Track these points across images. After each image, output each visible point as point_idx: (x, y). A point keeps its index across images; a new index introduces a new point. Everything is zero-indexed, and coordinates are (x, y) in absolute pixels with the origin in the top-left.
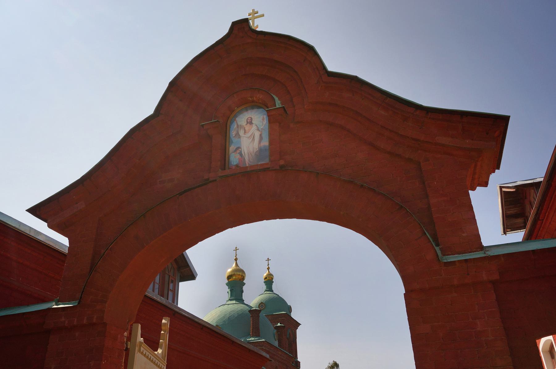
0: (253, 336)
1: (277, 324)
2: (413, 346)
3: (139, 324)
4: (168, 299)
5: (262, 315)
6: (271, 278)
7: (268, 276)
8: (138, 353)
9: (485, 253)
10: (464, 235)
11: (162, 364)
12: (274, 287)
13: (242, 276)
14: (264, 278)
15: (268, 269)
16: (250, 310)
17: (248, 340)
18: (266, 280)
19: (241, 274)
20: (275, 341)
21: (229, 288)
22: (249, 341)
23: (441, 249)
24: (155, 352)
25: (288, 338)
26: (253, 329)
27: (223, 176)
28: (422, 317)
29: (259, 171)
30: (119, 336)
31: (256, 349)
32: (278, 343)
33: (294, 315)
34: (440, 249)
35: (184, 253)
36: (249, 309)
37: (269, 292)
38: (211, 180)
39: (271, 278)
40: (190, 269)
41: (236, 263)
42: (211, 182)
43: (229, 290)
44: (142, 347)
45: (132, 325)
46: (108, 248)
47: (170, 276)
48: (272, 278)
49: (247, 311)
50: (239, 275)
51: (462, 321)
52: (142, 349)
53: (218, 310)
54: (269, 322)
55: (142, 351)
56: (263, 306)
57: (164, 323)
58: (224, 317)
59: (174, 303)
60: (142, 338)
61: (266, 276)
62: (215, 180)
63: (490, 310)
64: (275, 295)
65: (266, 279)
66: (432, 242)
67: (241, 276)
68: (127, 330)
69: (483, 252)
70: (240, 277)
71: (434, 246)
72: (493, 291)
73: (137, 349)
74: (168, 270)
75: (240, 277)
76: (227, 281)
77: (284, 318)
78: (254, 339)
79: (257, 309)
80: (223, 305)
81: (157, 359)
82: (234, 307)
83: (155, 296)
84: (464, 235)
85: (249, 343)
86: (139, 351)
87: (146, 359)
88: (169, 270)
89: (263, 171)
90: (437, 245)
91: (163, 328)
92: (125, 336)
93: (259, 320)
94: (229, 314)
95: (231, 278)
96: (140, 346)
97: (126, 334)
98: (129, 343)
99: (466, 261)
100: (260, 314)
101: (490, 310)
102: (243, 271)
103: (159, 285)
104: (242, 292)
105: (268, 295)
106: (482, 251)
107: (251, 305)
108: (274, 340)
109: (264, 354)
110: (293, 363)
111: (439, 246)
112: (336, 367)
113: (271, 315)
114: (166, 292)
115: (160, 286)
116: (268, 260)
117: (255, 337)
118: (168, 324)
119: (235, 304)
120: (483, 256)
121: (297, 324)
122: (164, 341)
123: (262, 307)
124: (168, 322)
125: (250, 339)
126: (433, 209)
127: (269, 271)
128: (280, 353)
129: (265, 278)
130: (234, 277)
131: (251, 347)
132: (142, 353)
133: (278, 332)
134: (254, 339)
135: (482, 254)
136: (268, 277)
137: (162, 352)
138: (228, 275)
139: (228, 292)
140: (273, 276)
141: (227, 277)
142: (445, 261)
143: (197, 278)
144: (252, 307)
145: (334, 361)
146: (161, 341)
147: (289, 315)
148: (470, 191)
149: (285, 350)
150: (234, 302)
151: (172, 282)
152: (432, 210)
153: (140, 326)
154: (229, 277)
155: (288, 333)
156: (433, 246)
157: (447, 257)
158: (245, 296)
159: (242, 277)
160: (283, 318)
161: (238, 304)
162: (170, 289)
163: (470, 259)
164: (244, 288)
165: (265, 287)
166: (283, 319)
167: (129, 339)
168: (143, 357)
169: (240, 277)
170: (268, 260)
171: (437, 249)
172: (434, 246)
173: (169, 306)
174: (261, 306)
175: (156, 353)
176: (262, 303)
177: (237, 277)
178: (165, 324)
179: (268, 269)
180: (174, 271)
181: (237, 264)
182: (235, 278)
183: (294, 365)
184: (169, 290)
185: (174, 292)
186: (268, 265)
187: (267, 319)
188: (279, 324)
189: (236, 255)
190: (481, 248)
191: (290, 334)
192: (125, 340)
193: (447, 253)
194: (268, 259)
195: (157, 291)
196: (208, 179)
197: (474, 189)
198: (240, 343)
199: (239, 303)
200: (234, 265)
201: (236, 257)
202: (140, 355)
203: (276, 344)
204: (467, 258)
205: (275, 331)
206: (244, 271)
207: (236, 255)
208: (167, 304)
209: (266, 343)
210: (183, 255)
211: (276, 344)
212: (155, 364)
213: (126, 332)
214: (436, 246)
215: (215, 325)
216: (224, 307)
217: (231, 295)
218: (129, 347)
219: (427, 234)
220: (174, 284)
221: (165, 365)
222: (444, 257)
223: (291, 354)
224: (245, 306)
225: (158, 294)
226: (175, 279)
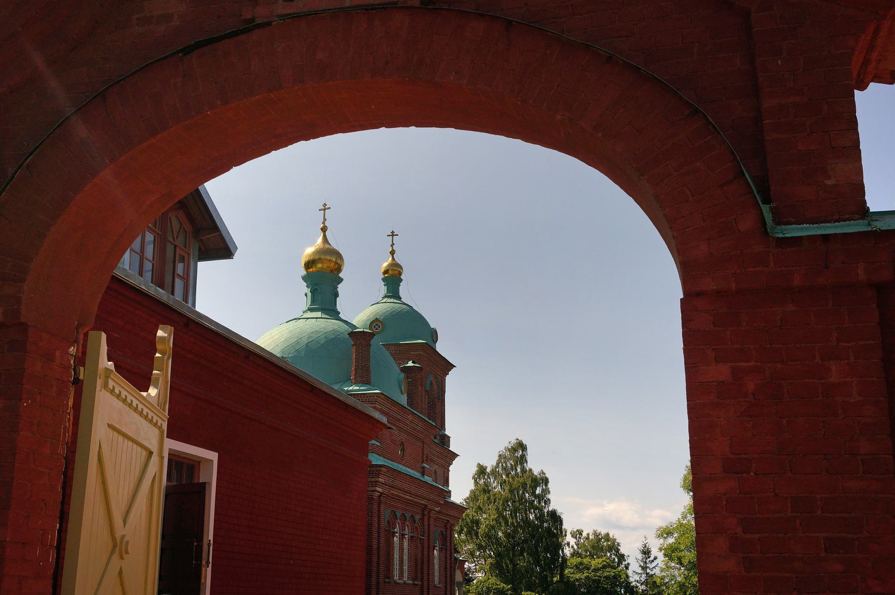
0: (356, 383)
1: (407, 363)
2: (688, 405)
3: (103, 333)
4: (173, 294)
5: (377, 343)
6: (396, 272)
7: (392, 268)
8: (102, 390)
9: (869, 225)
10: (829, 182)
11: (159, 416)
12: (403, 290)
13: (336, 263)
14: (383, 270)
15: (392, 253)
16: (352, 332)
17: (346, 389)
18: (386, 275)
19: (334, 259)
20: (402, 395)
21: (308, 287)
22: (348, 391)
23: (775, 212)
24: (142, 393)
25: (427, 391)
26: (356, 369)
27: (287, 15)
28: (714, 349)
29: (373, 9)
30: (58, 353)
31: (359, 405)
32: (408, 399)
33: (442, 348)
34: (772, 210)
35: (200, 188)
36: (350, 330)
37: (392, 300)
38: (259, 21)
39: (396, 272)
40: (221, 236)
41: (325, 236)
42: (259, 26)
43: (308, 291)
44: (112, 379)
45: (86, 335)
46: (22, 164)
47: (177, 248)
48: (400, 272)
49: (346, 333)
50: (330, 260)
51: (799, 362)
52: (111, 384)
53: (285, 328)
54: (390, 359)
55: (146, 414)
56: (379, 327)
57: (159, 337)
58: (297, 343)
59: (186, 302)
60: (111, 363)
61: (386, 267)
62: (269, 24)
63: (861, 343)
64: (404, 306)
65: (387, 273)
66: (755, 193)
67: (334, 263)
68: (75, 342)
69: (865, 222)
70: (332, 265)
71: (760, 201)
72: (875, 305)
73: (99, 382)
74: (173, 234)
75: (332, 265)
76: (304, 272)
77: (420, 353)
78: (358, 388)
79: (365, 330)
80: (295, 319)
81: (144, 405)
82: (320, 324)
83: (145, 284)
84: (829, 182)
85: (351, 395)
86: (105, 386)
87: (121, 404)
88: (175, 236)
89: (381, 8)
90: (766, 201)
91: (159, 346)
92: (72, 355)
93: (369, 352)
94: (309, 338)
95: (314, 266)
96: (107, 377)
97: (73, 350)
98: (82, 369)
99: (826, 238)
100: (372, 342)
101: (861, 343)
102: (338, 255)
103: (153, 264)
104: (336, 295)
105: (389, 305)
106: (863, 219)
107: (354, 323)
108: (400, 393)
109: (377, 415)
110: (435, 438)
111: (770, 204)
112: (520, 451)
113: (395, 345)
114: (168, 278)
115: (155, 265)
116: (393, 234)
117: (361, 384)
118: (169, 340)
119: (321, 318)
120: (865, 230)
121: (448, 366)
122: (163, 371)
123: (377, 329)
124: (169, 335)
125: (351, 388)
126: (767, 121)
127: (393, 257)
128: (410, 417)
129: (386, 272)
130: (320, 265)
131: (351, 401)
132: (112, 392)
133: (407, 377)
134: (358, 388)
135: (863, 227)
136: (392, 270)
137: (159, 394)
138: (307, 259)
139: (306, 295)
140: (402, 268)
141: (305, 264)
142: (780, 236)
143: (237, 255)
144: (356, 328)
145: (517, 439)
146: (155, 372)
147: (432, 346)
148: (855, 91)
149: (421, 413)
150: (319, 314)
151: (182, 259)
152: (764, 122)
153: (104, 336)
154: (309, 265)
155: (429, 382)
156: (757, 201)
157: (784, 227)
158: (342, 304)
159: (337, 266)
160: (418, 353)
161: (327, 318)
162: (178, 275)
163: (836, 235)
164: (341, 288)
165: (383, 290)
166: (418, 354)
167: (81, 360)
168: (115, 399)
169: (332, 266)
170: (393, 234)
171: (765, 208)
172: (760, 201)
173: (176, 307)
174: (375, 327)
175: (144, 394)
176: (377, 320)
177: (325, 266)
178: (162, 338)
179: (392, 253)
180: (186, 238)
181: (325, 239)
182: (321, 268)
183: (436, 441)
184: (176, 276)
185: (185, 281)
186: (393, 245)
187: (386, 351)
188: (410, 364)
189: (325, 220)
190: (863, 211)
191: (431, 383)
192: (72, 362)
193: (785, 220)
194: (393, 232)
195: (148, 275)
196: (253, 20)
197: (863, 87)
198: (327, 391)
199: (329, 317)
200: (320, 240)
201: (324, 223)
202: (108, 395)
203: (403, 400)
204: (828, 233)
205: (402, 375)
206: (341, 255)
207: (325, 220)
208: (171, 303)
209: (383, 397)
210: (198, 192)
211: (403, 400)
212: (152, 424)
213: (74, 347)
214: (763, 203)
215: (277, 352)
216: (296, 323)
217: (313, 301)
218: (81, 377)
219: (747, 176)
220: (186, 265)
221: (165, 420)
222: (779, 228)
223: (432, 421)
224: (342, 324)
225: (152, 283)
226: (189, 254)
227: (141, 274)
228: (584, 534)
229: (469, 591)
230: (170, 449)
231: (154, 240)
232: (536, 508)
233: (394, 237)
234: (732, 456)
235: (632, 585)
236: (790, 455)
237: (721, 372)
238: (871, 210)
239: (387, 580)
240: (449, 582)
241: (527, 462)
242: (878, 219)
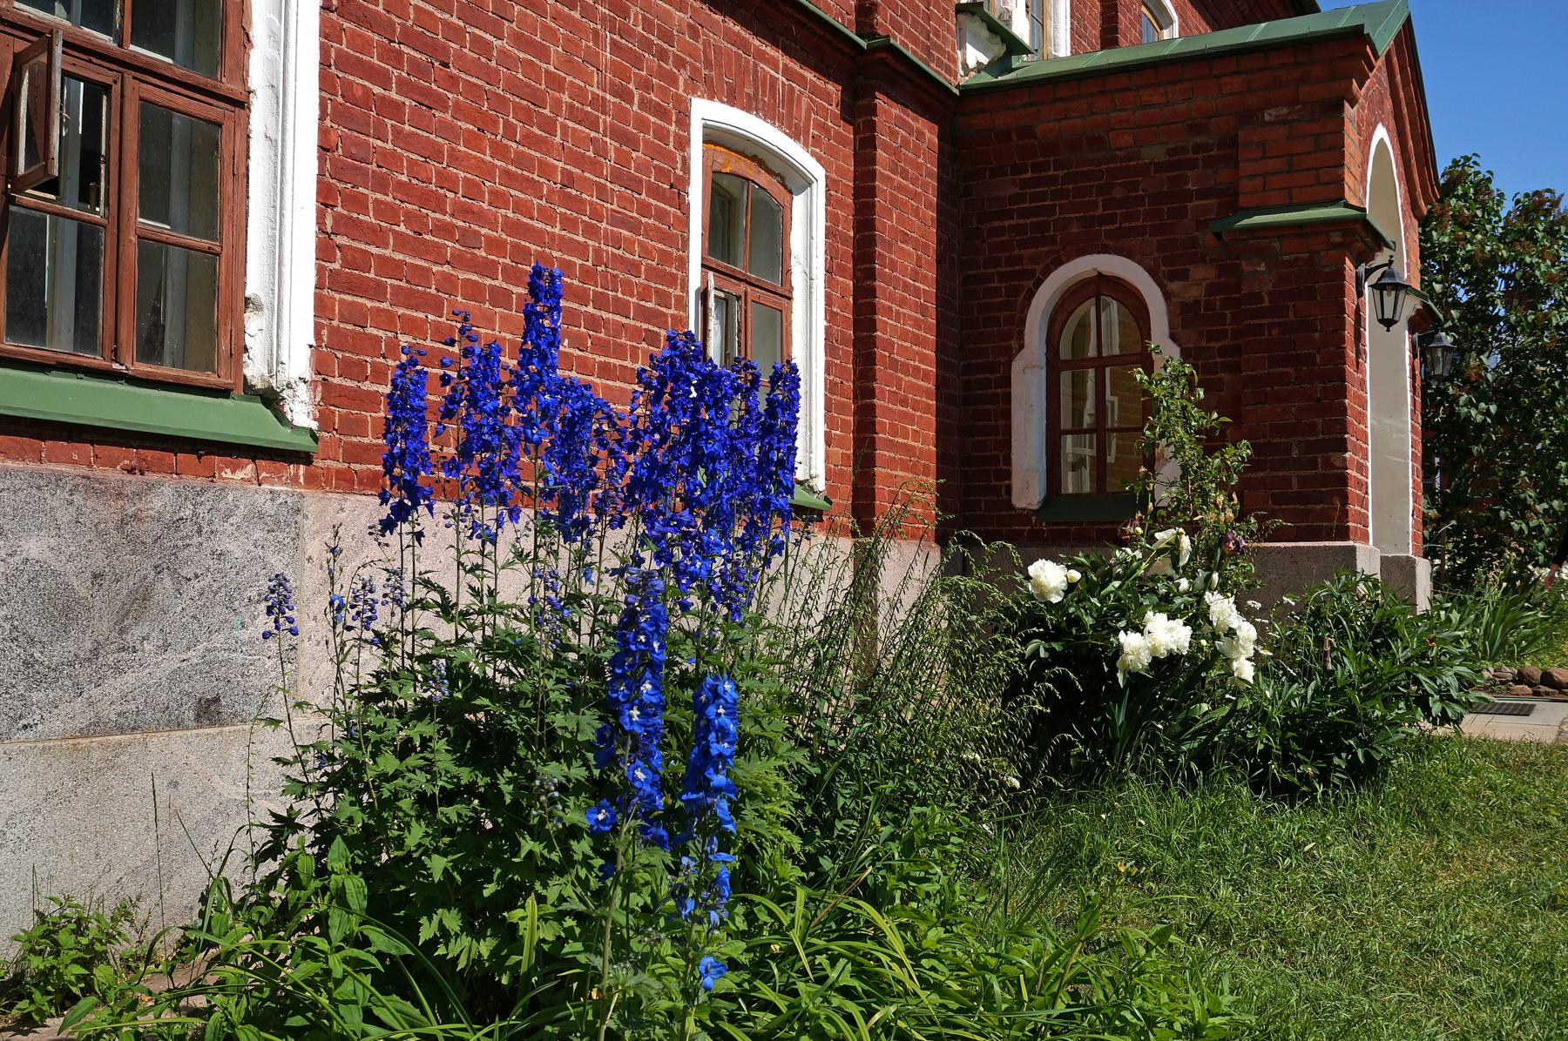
139: (1548, 191)
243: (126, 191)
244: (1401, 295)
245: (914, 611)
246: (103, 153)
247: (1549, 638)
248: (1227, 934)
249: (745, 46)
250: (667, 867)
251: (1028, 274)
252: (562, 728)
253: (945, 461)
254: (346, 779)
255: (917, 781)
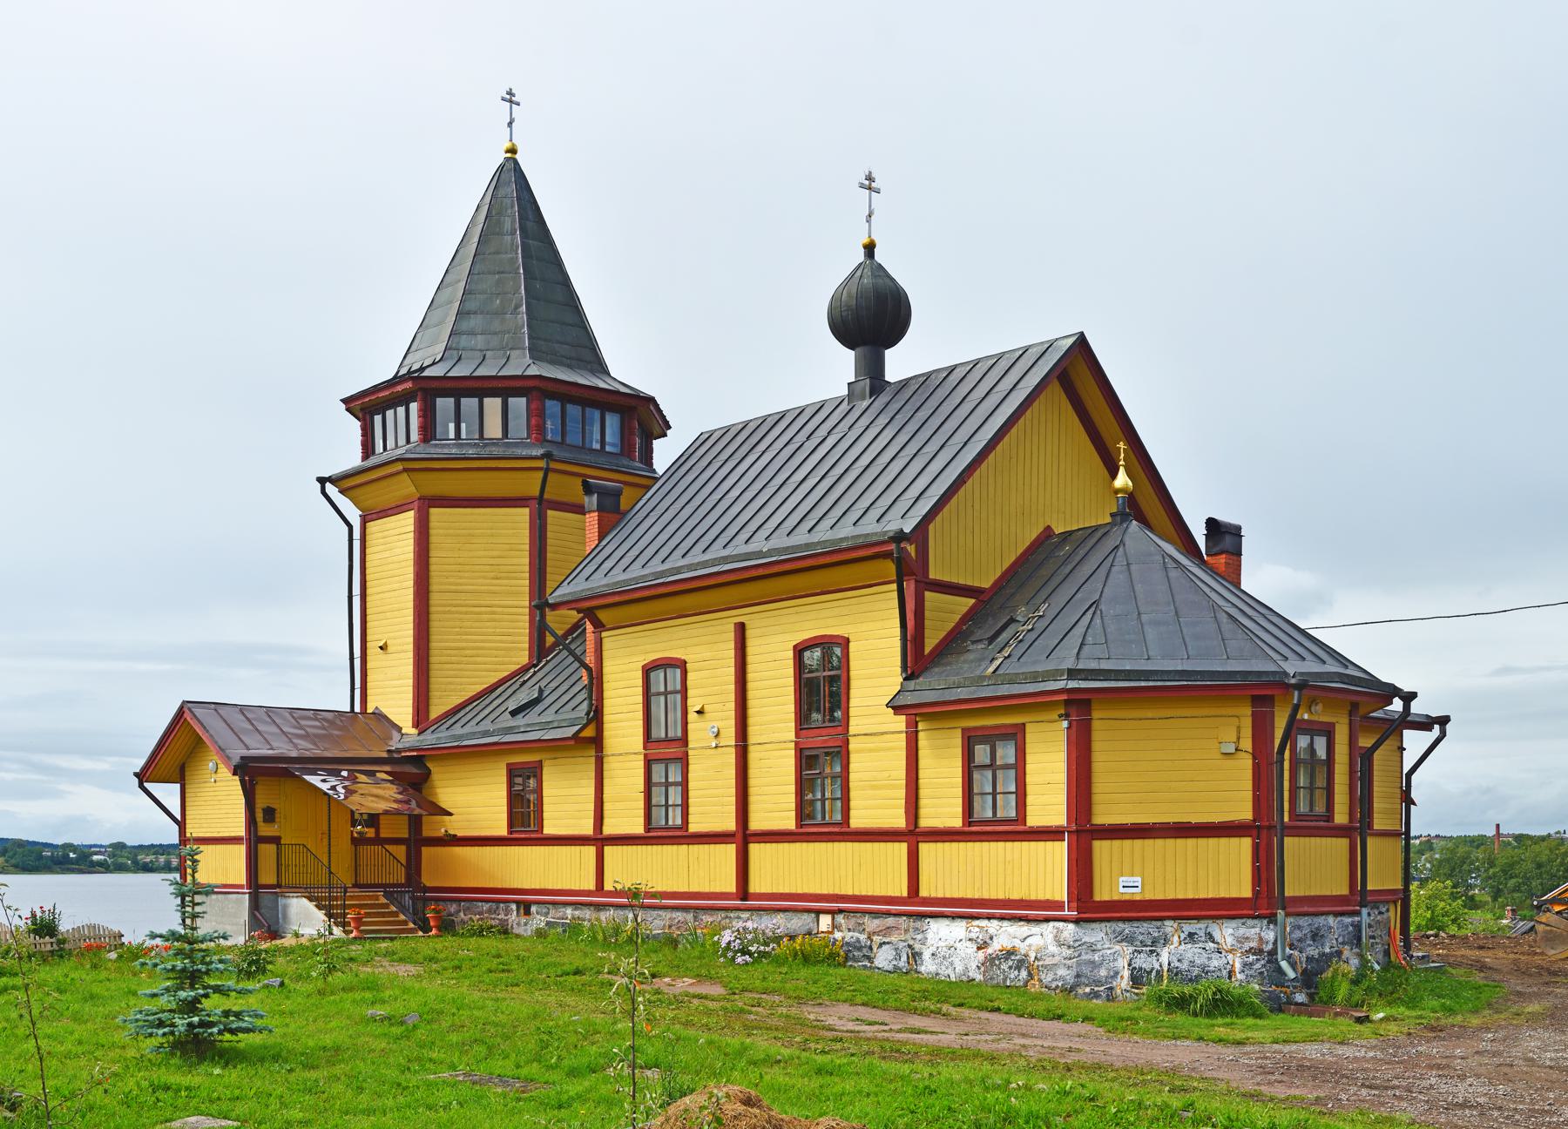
139: (216, 932)
227: (1324, 662)
228: (123, 939)
229: (1233, 1126)
230: (377, 708)
231: (1174, 918)
232: (698, 1047)
233: (755, 849)
234: (1298, 749)
235: (197, 1005)
236: (42, 1070)
237: (267, 817)
238: (886, 379)
239: (545, 1037)
240: (1561, 1069)
241: (1124, 545)
242: (946, 1030)
243: (1066, 585)
244: (668, 670)
245: (1004, 952)
246: (415, 754)
247: (391, 982)
248: (1362, 975)
249: (513, 207)
250: (1196, 934)
251: (239, 721)
252: (632, 885)
253: (1305, 897)
254: (213, 1059)
255: (1511, 877)
